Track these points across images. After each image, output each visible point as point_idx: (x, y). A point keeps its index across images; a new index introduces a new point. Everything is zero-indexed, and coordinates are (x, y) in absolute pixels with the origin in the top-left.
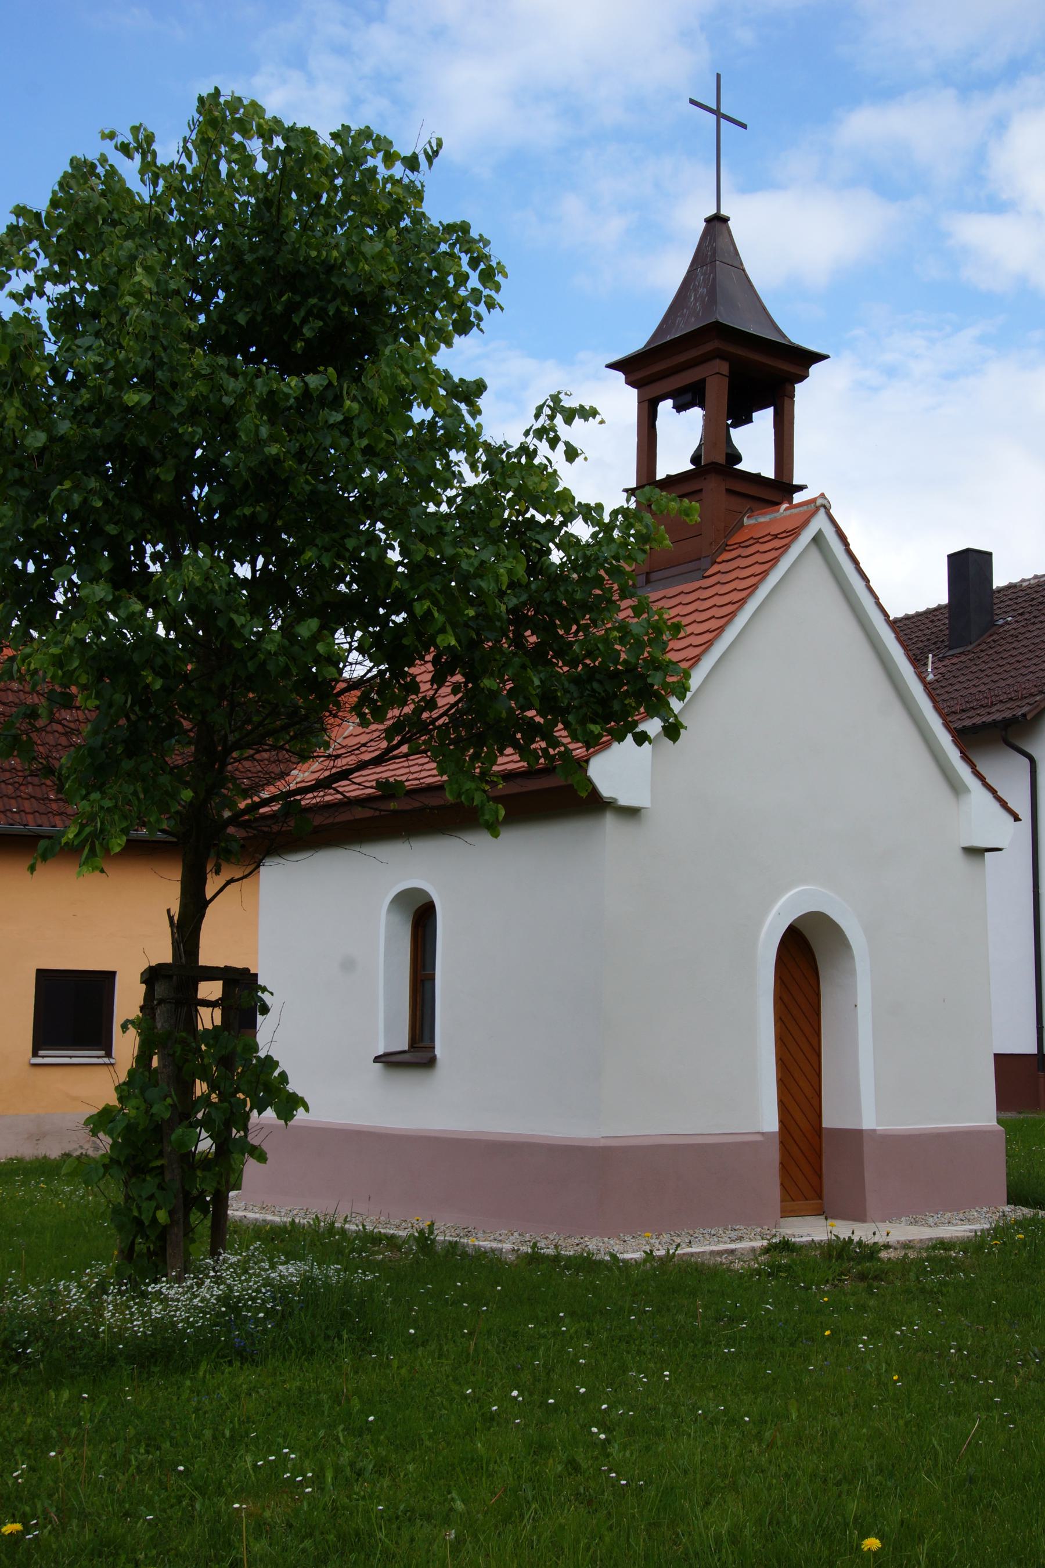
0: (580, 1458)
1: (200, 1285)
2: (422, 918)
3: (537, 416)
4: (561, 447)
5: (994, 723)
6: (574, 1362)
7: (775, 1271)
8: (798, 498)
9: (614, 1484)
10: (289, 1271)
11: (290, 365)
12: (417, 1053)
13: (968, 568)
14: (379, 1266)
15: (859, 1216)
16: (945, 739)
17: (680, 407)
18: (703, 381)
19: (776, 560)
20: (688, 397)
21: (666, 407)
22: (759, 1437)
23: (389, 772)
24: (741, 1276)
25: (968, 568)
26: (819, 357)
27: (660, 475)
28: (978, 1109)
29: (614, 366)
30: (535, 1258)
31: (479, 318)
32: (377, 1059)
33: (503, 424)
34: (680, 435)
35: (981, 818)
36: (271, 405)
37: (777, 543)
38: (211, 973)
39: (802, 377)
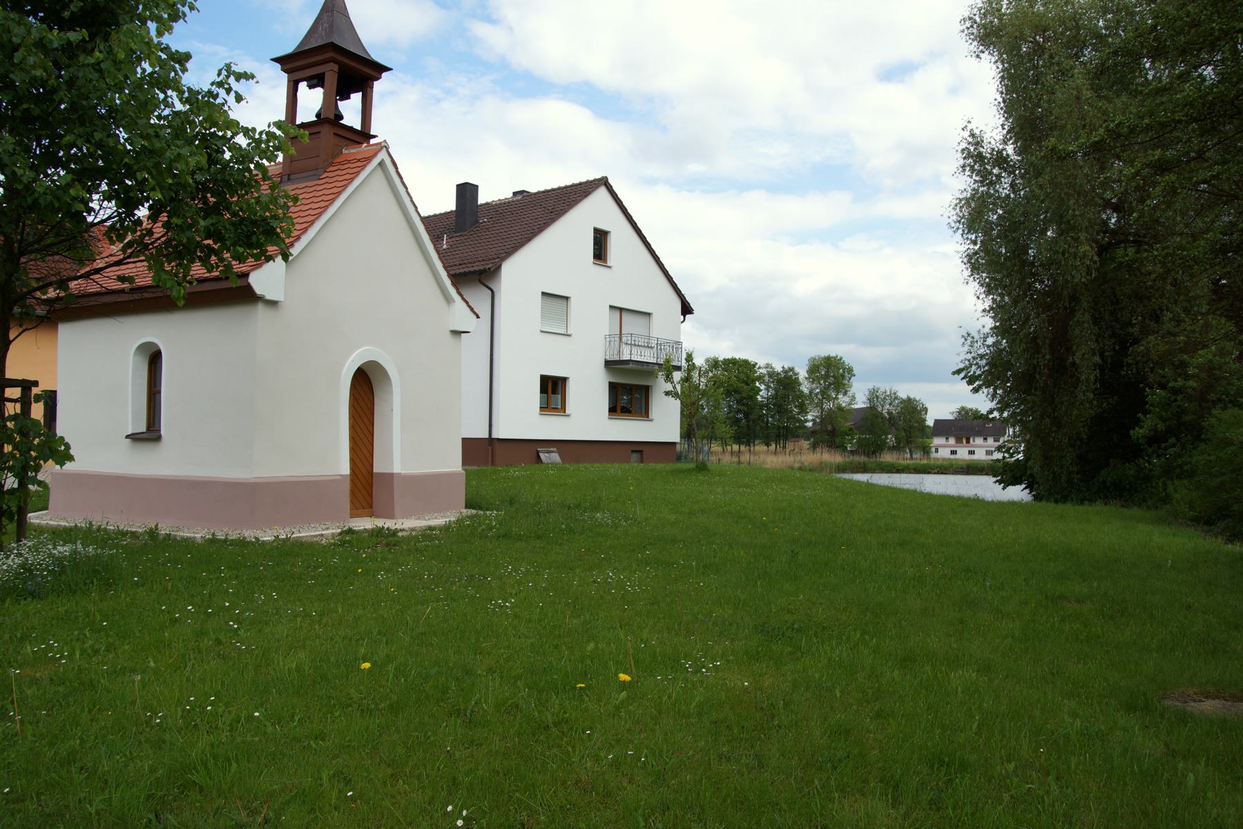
0: (222, 637)
1: (7, 558)
2: (154, 359)
3: (219, 75)
4: (233, 94)
5: (475, 272)
6: (227, 591)
7: (343, 543)
8: (372, 141)
9: (239, 648)
10: (64, 549)
11: (65, 26)
12: (151, 433)
13: (466, 192)
14: (123, 547)
15: (391, 516)
16: (443, 274)
17: (311, 87)
18: (323, 74)
19: (358, 173)
20: (315, 82)
21: (303, 86)
22: (320, 622)
23: (125, 270)
24: (324, 547)
25: (466, 192)
26: (387, 69)
27: (298, 122)
28: (453, 463)
29: (276, 60)
30: (213, 541)
31: (185, 15)
32: (127, 437)
33: (198, 77)
34: (311, 101)
35: (459, 315)
36: (41, 45)
37: (359, 164)
38: (13, 383)
39: (378, 78)
